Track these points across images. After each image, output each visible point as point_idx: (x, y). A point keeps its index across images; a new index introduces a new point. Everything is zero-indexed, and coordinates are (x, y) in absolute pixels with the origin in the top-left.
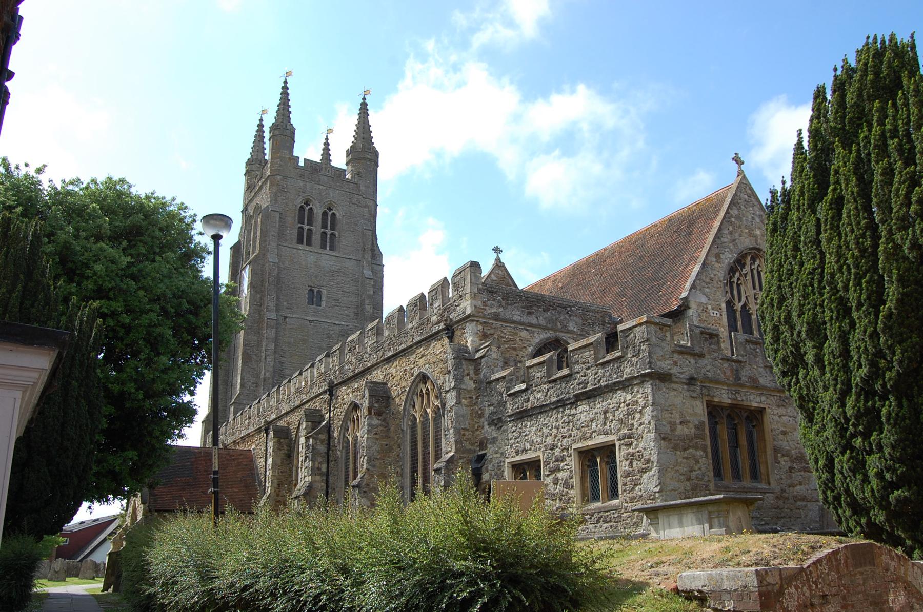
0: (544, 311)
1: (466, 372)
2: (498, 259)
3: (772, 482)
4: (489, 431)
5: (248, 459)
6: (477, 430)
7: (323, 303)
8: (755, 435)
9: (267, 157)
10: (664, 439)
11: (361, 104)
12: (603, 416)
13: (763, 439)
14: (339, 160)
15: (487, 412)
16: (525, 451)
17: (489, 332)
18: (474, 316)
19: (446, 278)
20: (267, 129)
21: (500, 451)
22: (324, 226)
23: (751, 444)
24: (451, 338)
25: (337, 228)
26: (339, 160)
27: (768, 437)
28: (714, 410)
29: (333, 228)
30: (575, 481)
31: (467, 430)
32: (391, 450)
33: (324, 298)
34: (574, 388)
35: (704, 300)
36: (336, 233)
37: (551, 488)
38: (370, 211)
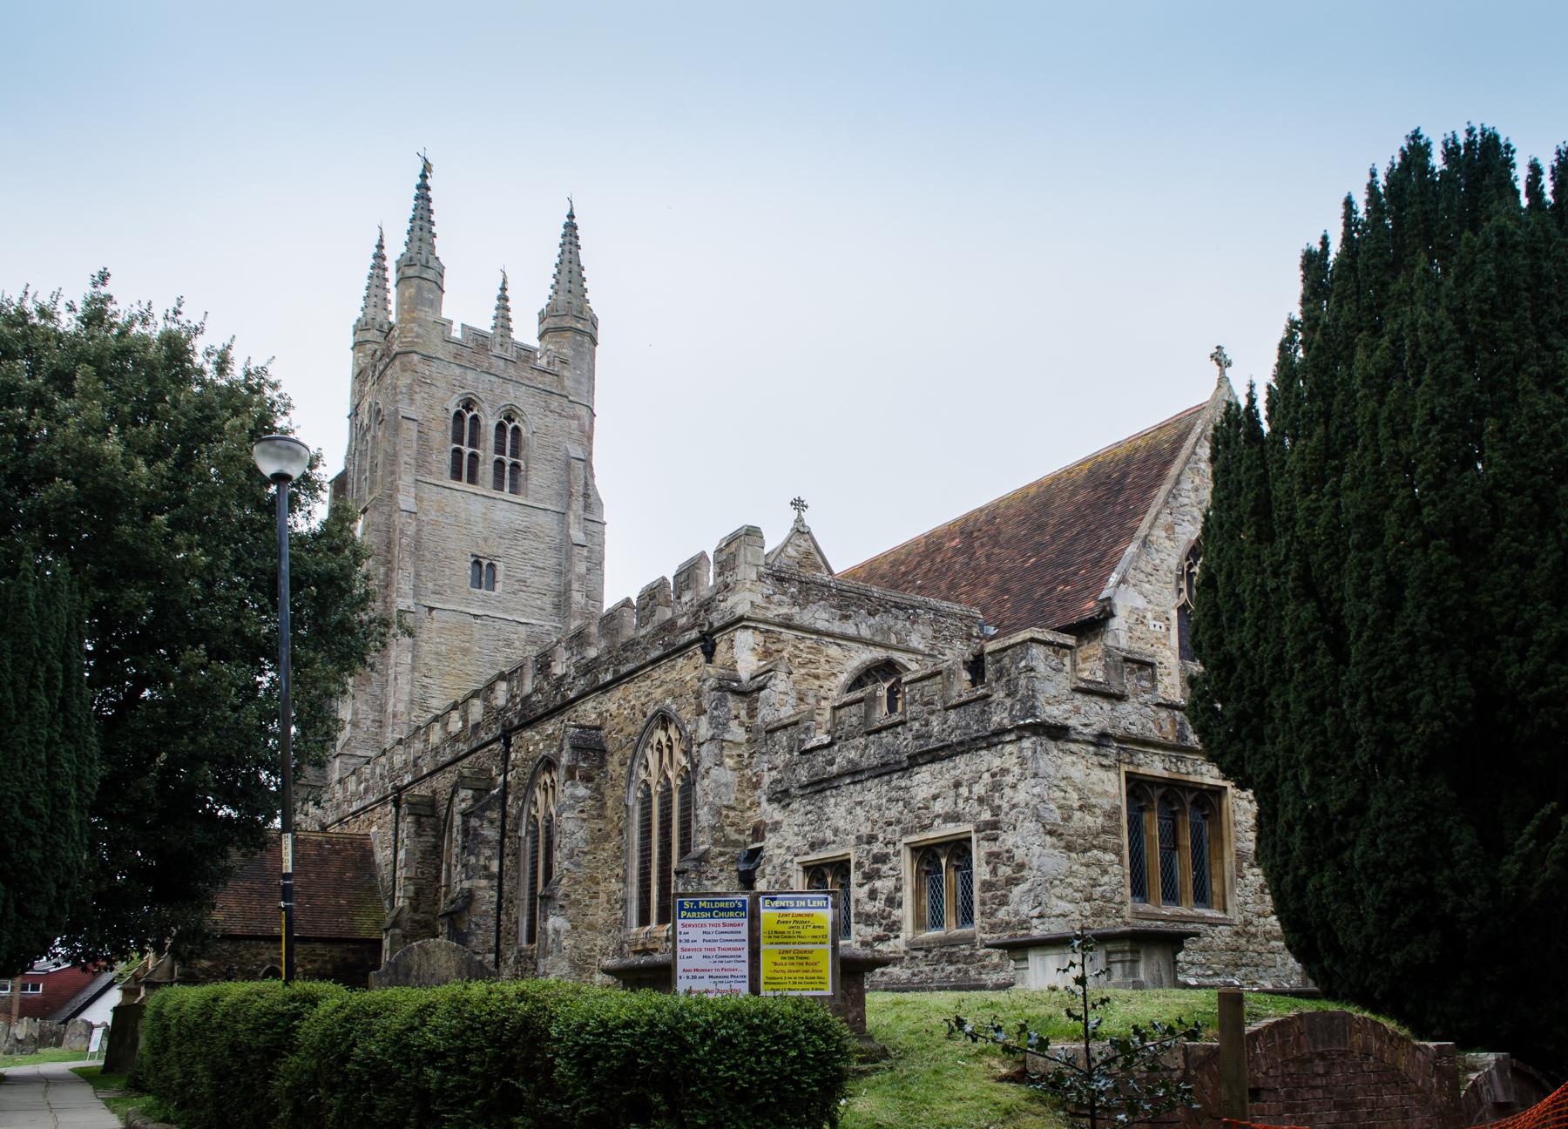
1: (734, 712)
2: (799, 520)
3: (1229, 906)
4: (770, 812)
5: (361, 851)
7: (499, 586)
8: (1207, 830)
10: (1051, 833)
13: (1219, 838)
14: (526, 331)
15: (767, 779)
16: (823, 843)
17: (774, 647)
18: (749, 619)
19: (664, 579)
20: (391, 264)
21: (786, 844)
22: (500, 449)
26: (526, 331)
28: (1138, 787)
29: (515, 454)
30: (907, 895)
31: (734, 809)
33: (500, 576)
34: (906, 742)
35: (1140, 602)
36: (522, 463)
37: (870, 907)
38: (581, 426)
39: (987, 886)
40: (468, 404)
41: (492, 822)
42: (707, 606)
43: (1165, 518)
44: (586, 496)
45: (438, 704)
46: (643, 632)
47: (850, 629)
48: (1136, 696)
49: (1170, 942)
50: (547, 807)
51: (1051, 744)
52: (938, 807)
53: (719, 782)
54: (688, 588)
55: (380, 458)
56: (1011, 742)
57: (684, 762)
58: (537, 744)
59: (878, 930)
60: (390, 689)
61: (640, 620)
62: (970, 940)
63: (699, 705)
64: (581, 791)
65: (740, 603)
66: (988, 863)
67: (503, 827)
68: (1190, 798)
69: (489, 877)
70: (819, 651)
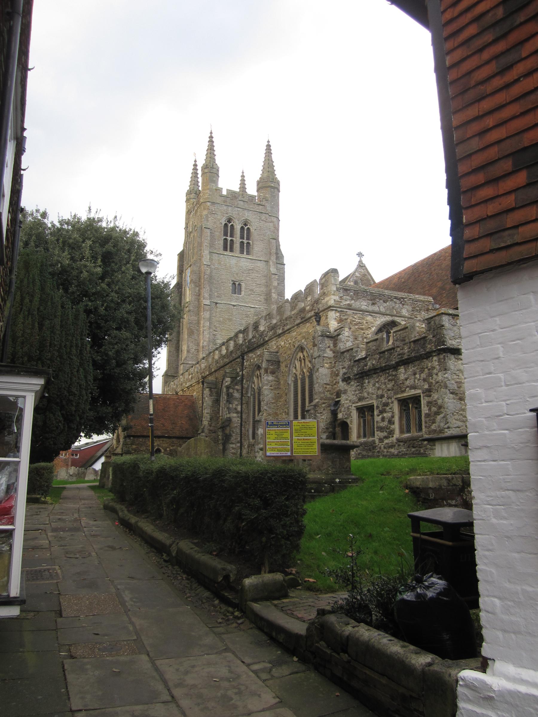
0: (384, 302)
1: (328, 345)
2: (360, 261)
4: (342, 385)
6: (335, 384)
7: (243, 293)
9: (200, 188)
10: (452, 393)
11: (241, 180)
12: (413, 377)
14: (252, 190)
15: (342, 372)
17: (344, 318)
20: (199, 168)
21: (349, 399)
22: (242, 237)
24: (318, 322)
25: (251, 238)
26: (252, 190)
29: (248, 239)
30: (396, 419)
31: (328, 385)
32: (281, 397)
33: (243, 289)
37: (382, 424)
38: (274, 225)
39: (427, 415)
40: (229, 221)
41: (237, 390)
42: (317, 302)
44: (277, 254)
45: (219, 342)
46: (293, 313)
50: (258, 384)
51: (452, 356)
52: (408, 383)
53: (323, 373)
54: (310, 295)
55: (196, 245)
57: (310, 365)
58: (254, 359)
59: (385, 434)
60: (201, 337)
63: (314, 343)
64: (271, 378)
65: (331, 300)
66: (427, 406)
67: (242, 393)
69: (237, 412)
70: (363, 319)
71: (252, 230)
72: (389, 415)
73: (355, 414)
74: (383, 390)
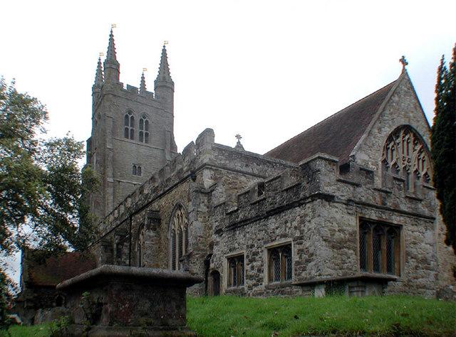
1: (202, 200)
2: (239, 143)
4: (215, 237)
10: (325, 240)
14: (150, 87)
23: (389, 248)
26: (150, 87)
27: (403, 244)
28: (364, 223)
29: (146, 130)
30: (266, 268)
33: (142, 171)
37: (251, 273)
39: (298, 263)
42: (193, 162)
43: (378, 125)
47: (249, 170)
48: (365, 185)
49: (382, 283)
53: (197, 226)
56: (309, 202)
59: (254, 282)
61: (171, 169)
62: (290, 285)
64: (152, 234)
65: (205, 159)
68: (387, 229)
71: (150, 122)
72: (259, 263)
73: (225, 263)
74: (253, 240)
